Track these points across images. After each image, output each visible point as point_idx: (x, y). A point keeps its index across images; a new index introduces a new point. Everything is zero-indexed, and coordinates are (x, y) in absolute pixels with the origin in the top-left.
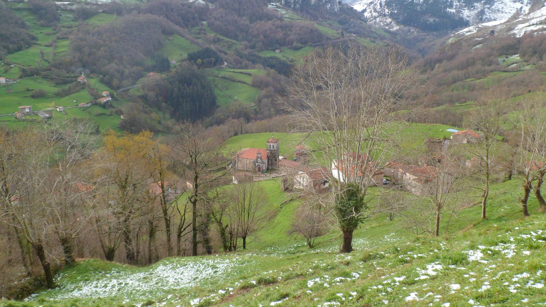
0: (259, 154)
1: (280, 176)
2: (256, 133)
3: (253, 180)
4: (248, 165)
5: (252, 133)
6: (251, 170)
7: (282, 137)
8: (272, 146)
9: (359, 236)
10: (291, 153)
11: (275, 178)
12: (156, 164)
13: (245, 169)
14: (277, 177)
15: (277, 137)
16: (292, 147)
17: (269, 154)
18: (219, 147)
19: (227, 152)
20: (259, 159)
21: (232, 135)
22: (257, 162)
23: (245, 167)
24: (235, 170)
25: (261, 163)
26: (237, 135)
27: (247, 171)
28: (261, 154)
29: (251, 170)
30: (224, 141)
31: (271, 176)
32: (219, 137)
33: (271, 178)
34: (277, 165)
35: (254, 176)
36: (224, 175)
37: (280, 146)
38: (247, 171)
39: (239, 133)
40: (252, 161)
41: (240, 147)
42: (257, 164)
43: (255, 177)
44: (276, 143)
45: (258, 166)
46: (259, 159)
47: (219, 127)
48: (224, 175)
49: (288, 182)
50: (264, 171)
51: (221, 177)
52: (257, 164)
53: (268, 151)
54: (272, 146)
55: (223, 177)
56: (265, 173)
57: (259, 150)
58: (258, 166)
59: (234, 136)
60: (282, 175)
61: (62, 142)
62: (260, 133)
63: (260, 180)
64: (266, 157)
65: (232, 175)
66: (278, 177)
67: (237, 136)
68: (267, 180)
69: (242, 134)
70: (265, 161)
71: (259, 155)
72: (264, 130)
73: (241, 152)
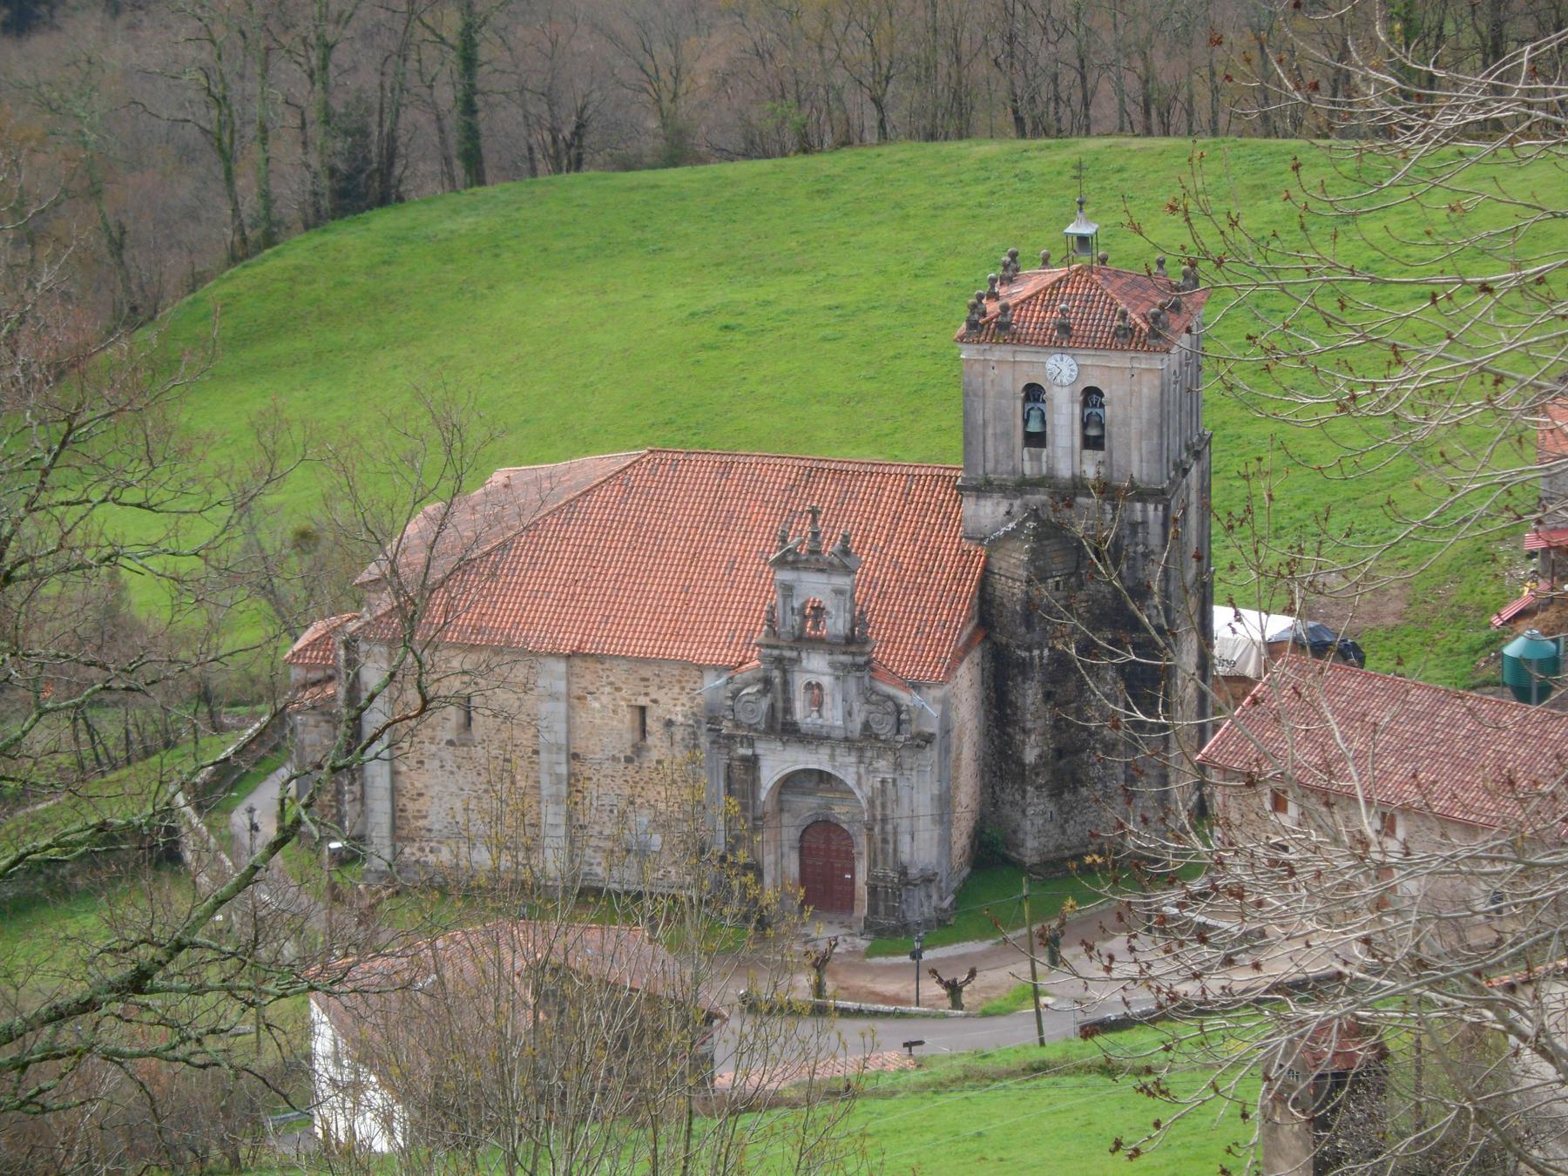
0: (812, 560)
1: (1230, 1004)
2: (754, 149)
3: (703, 1064)
4: (605, 788)
5: (677, 153)
6: (672, 872)
7: (1259, 216)
8: (1064, 417)
9: (1068, 945)
10: (1455, 545)
11: (1145, 1040)
12: (1352, 26)
13: (552, 862)
14: (1170, 1010)
15: (1168, 233)
16: (1471, 408)
17: (1014, 563)
18: (42, 439)
19: (202, 531)
20: (816, 666)
21: (289, 208)
22: (785, 729)
23: (553, 817)
24: (352, 879)
25: (864, 741)
26: (387, 196)
27: (589, 896)
28: (844, 562)
29: (672, 872)
30: (136, 314)
31: (1058, 989)
32: (30, 238)
33: (1062, 1040)
34: (1181, 790)
35: (723, 992)
36: (138, 982)
37: (1217, 413)
38: (589, 896)
39: (420, 167)
40: (674, 705)
41: (451, 431)
42: (777, 762)
43: (736, 1026)
44: (1154, 336)
45: (807, 806)
46: (816, 666)
47: (39, 43)
48: (138, 982)
49: (1398, 1110)
50: (920, 907)
51: (67, 1036)
52: (777, 762)
53: (988, 513)
54: (1064, 417)
55: (113, 1034)
56: (943, 927)
57: (826, 493)
58: (807, 806)
59: (315, 220)
60: (1280, 966)
61: (183, 369)
62: (827, 163)
63: (839, 1067)
64: (958, 617)
65: (297, 984)
66: (1201, 1010)
67: (383, 221)
68: (977, 1078)
69: (477, 177)
70: (926, 708)
71: (814, 587)
72: (903, 98)
73: (465, 524)
